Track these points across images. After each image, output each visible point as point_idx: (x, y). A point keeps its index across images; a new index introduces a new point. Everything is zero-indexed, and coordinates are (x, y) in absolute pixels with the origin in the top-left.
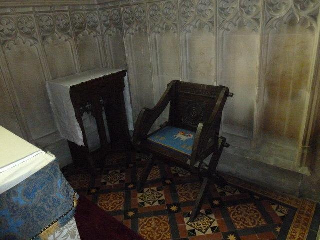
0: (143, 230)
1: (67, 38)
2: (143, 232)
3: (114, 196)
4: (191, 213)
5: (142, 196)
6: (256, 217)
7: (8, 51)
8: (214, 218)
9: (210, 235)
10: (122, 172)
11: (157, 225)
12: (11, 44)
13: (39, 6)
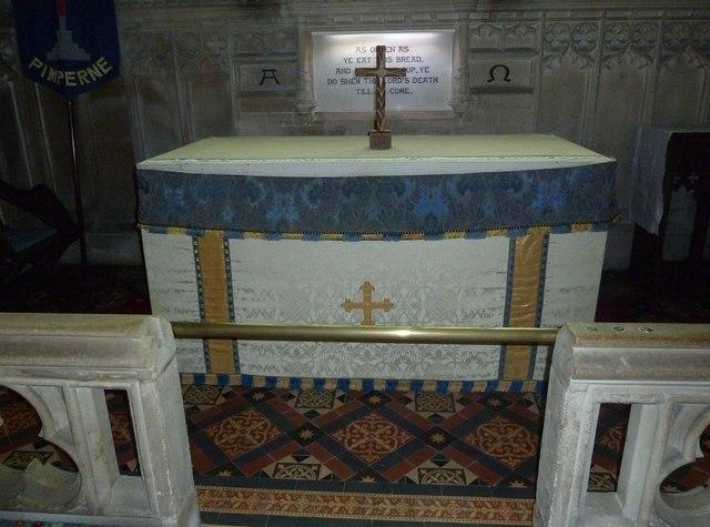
1: (703, 62)
6: (389, 432)
7: (605, 70)
12: (614, 61)
13: (366, 14)
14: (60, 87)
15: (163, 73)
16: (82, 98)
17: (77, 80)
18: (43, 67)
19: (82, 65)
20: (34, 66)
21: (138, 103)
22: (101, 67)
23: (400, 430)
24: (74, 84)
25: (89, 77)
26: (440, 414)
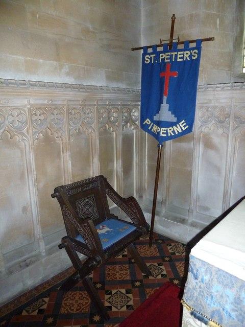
0: (87, 301)
2: (87, 299)
3: (72, 308)
4: (143, 274)
5: (109, 298)
8: (164, 269)
9: (113, 289)
10: (127, 292)
11: (116, 275)
14: (157, 136)
15: (220, 131)
16: (168, 143)
17: (167, 133)
18: (150, 124)
19: (172, 124)
20: (146, 123)
21: (200, 150)
22: (182, 126)
23: (177, 266)
24: (165, 135)
25: (174, 132)
26: (41, 308)
